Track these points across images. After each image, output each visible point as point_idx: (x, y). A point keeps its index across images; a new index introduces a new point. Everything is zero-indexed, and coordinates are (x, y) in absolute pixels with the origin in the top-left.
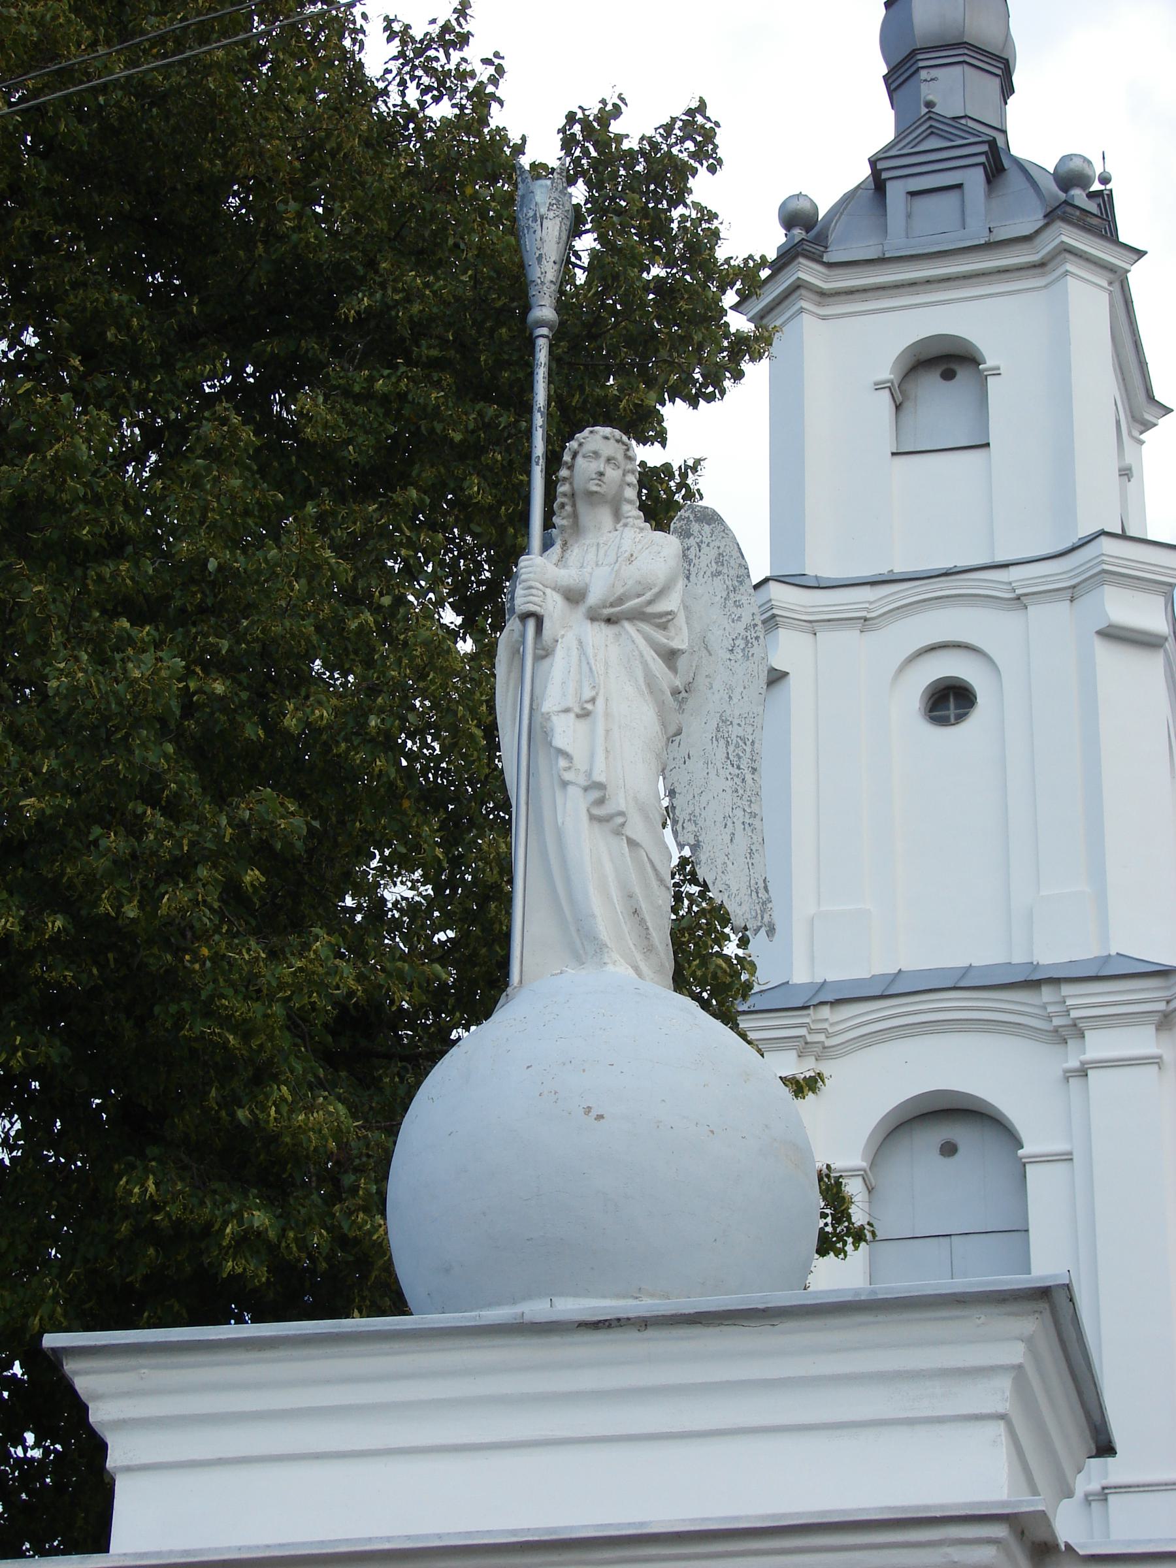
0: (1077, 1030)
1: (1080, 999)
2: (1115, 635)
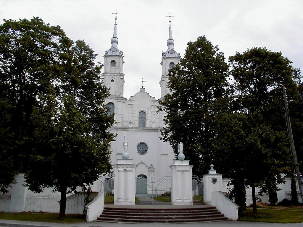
0: (118, 100)
1: (118, 98)
2: (121, 78)
